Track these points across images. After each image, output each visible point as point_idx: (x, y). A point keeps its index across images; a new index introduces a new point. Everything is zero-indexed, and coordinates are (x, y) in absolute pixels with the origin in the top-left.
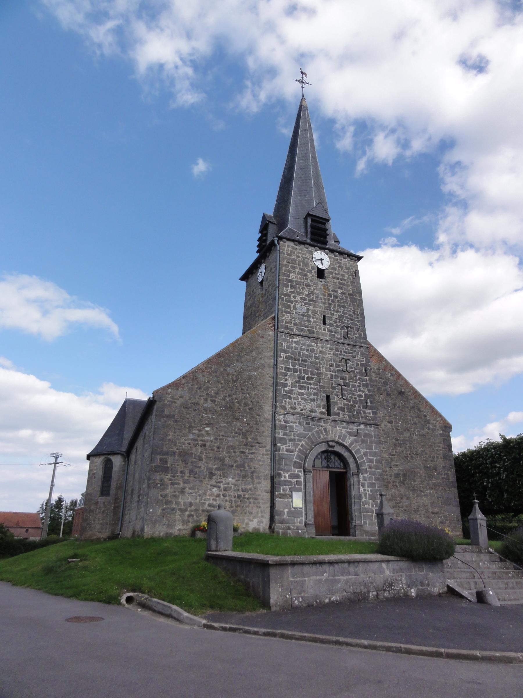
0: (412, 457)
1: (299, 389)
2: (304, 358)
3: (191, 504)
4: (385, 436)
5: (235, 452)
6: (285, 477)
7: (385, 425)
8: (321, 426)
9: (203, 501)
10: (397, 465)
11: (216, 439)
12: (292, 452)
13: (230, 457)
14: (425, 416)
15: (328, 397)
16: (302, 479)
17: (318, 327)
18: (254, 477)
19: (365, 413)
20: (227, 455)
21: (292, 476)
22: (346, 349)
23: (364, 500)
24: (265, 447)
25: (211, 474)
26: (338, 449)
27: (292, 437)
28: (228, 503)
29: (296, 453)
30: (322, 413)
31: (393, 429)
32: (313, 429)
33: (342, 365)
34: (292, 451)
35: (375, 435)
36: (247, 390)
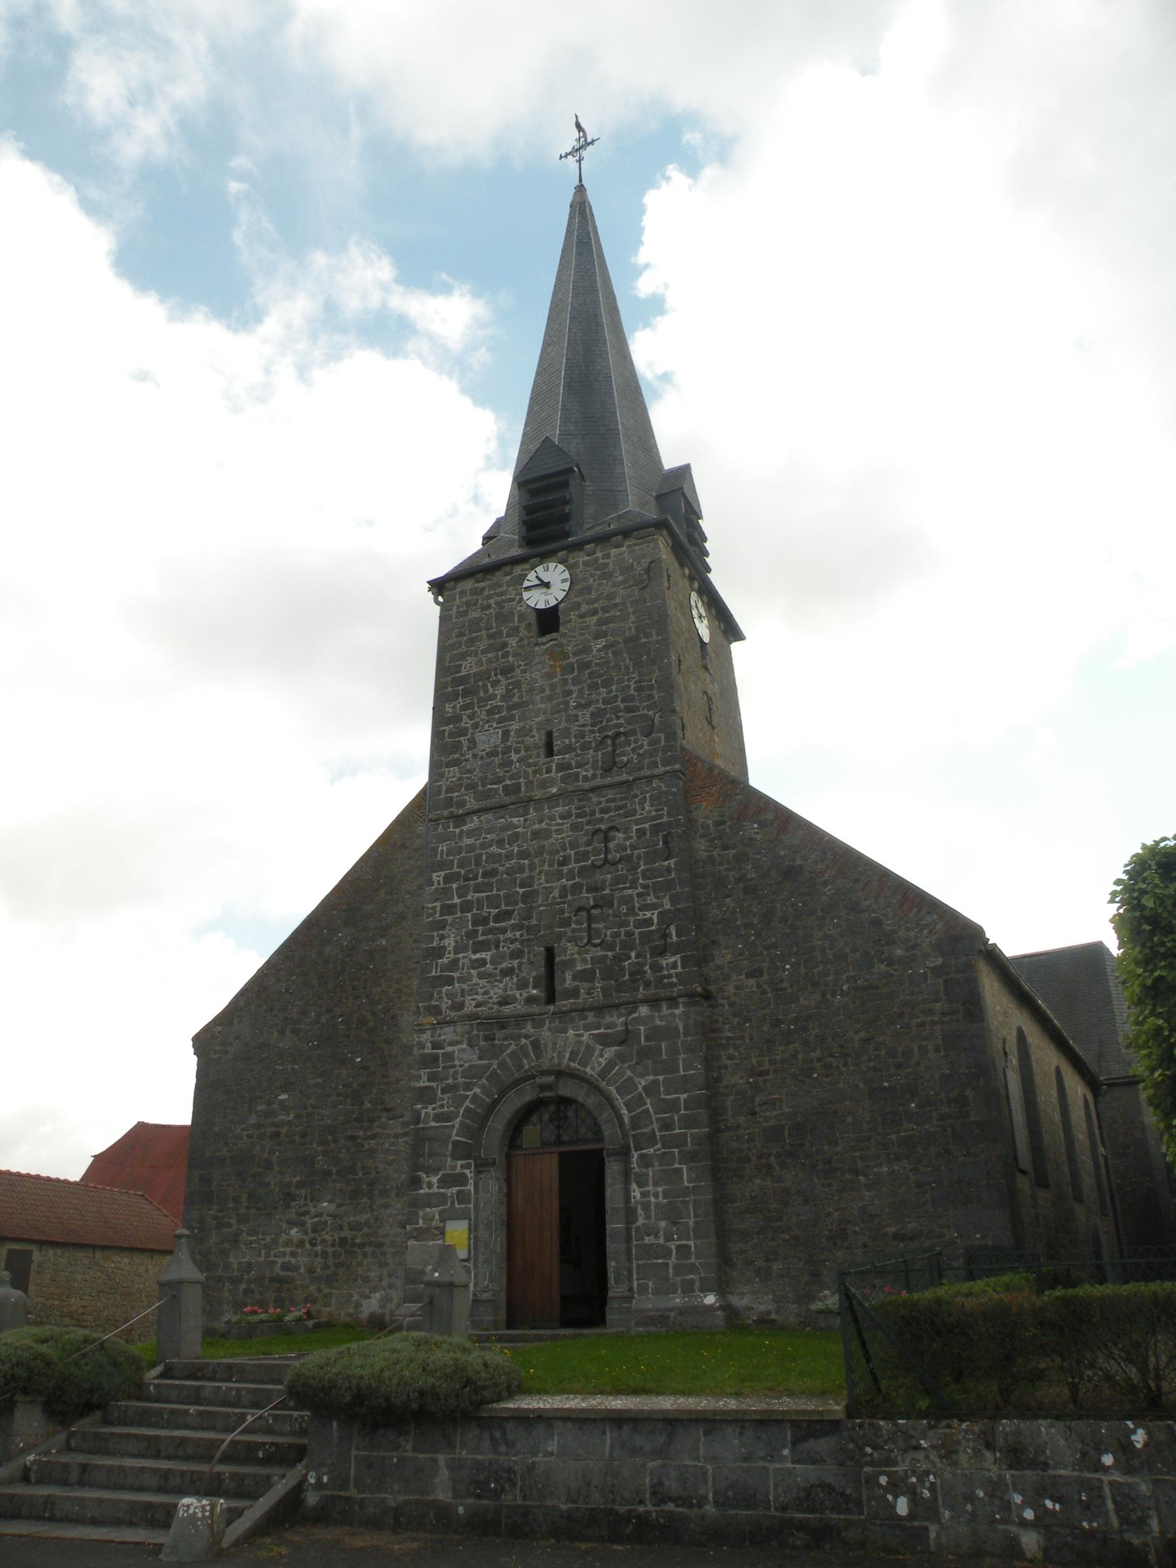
0: (828, 1066)
1: (475, 952)
2: (489, 867)
3: (250, 1266)
4: (736, 1021)
5: (335, 1141)
6: (430, 1185)
7: (737, 988)
8: (526, 1037)
9: (272, 1258)
10: (772, 1103)
11: (299, 1116)
12: (449, 1119)
13: (325, 1153)
14: (877, 923)
15: (550, 954)
16: (471, 1187)
17: (530, 770)
18: (376, 1193)
19: (656, 968)
20: (319, 1149)
21: (446, 1182)
22: (608, 801)
23: (641, 1221)
24: (402, 1116)
25: (289, 1197)
26: (566, 1089)
27: (450, 1081)
28: (319, 1259)
29: (457, 1122)
30: (530, 1000)
31: (764, 992)
32: (502, 1049)
33: (595, 849)
34: (448, 1117)
35: (686, 1027)
36: (365, 987)
